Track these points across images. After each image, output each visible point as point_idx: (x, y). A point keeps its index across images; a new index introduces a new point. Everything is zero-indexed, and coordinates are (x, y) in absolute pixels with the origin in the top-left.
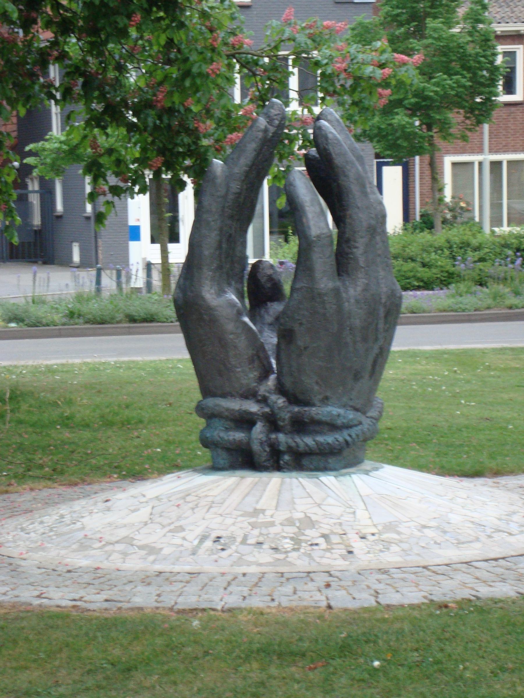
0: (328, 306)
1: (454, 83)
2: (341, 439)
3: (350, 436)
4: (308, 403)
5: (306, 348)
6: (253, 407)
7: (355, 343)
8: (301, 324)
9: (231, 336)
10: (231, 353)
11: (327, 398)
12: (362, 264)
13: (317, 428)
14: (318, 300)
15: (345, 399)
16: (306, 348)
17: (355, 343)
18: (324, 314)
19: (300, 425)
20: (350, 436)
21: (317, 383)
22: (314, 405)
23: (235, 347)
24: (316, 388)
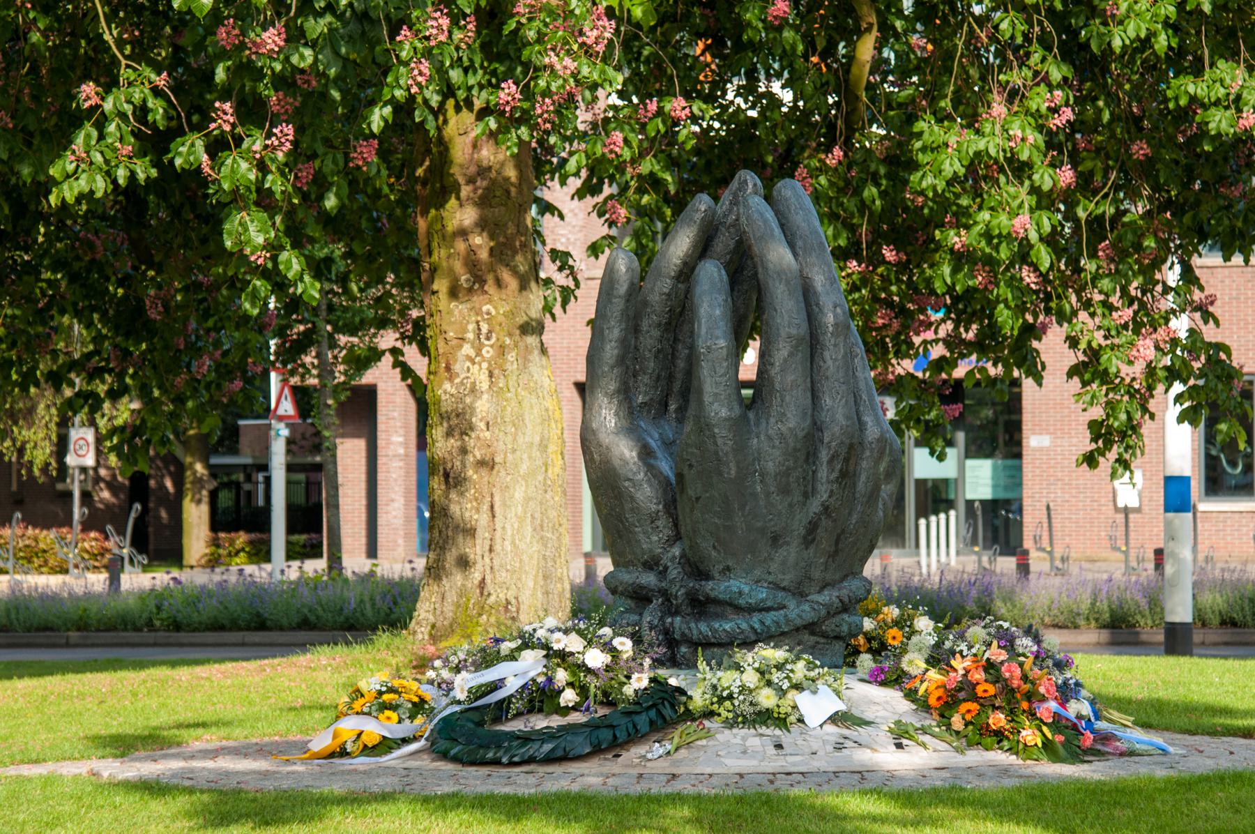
0: (720, 441)
1: (404, 109)
2: (744, 626)
3: (762, 623)
4: (707, 576)
5: (698, 499)
6: (649, 579)
7: (768, 494)
8: (690, 466)
9: (627, 484)
10: (628, 506)
11: (728, 569)
12: (777, 386)
13: (719, 609)
14: (707, 433)
15: (757, 572)
16: (698, 499)
17: (768, 494)
18: (716, 453)
19: (701, 606)
20: (762, 623)
21: (714, 547)
22: (713, 578)
23: (632, 498)
24: (714, 554)
